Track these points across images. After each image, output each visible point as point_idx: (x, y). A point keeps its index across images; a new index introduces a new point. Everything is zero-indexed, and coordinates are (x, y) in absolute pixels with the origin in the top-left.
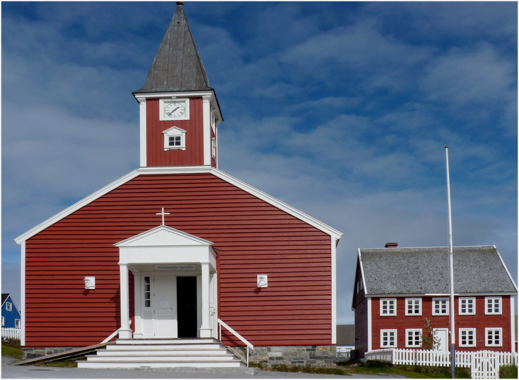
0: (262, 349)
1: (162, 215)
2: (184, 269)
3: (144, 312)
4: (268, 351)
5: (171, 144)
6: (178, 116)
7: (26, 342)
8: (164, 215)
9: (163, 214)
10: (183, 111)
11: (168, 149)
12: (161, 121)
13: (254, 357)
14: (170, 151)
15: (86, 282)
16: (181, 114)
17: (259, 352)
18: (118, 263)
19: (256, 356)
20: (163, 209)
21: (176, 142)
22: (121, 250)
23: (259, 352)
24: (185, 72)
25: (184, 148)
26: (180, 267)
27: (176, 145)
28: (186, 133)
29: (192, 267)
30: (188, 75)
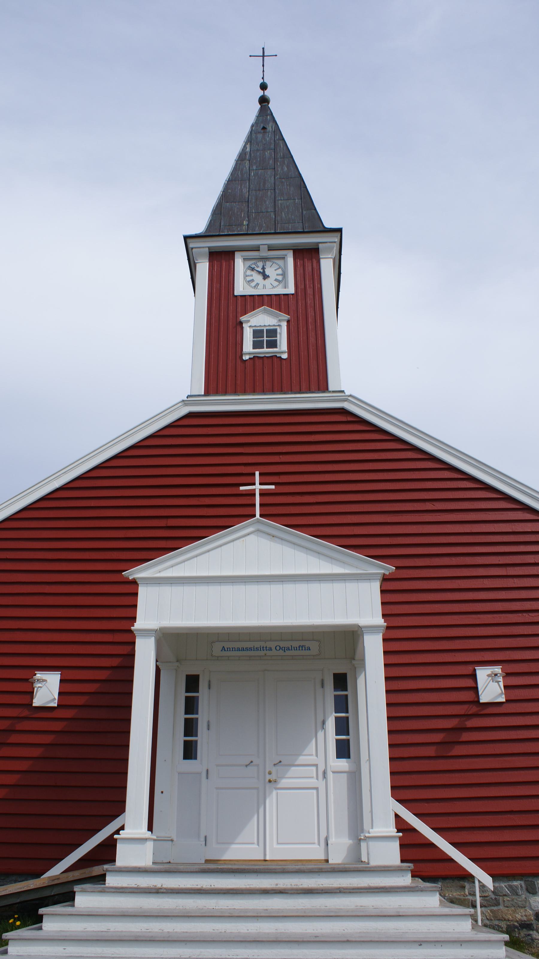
0: (511, 887)
1: (255, 490)
2: (288, 653)
3: (179, 773)
4: (530, 893)
5: (257, 345)
6: (271, 287)
7: (136, 594)
8: (260, 490)
9: (258, 487)
10: (280, 278)
11: (252, 356)
12: (236, 296)
13: (491, 911)
14: (255, 359)
15: (37, 685)
16: (277, 283)
17: (505, 895)
18: (132, 628)
19: (495, 908)
20: (257, 473)
21: (266, 340)
22: (142, 591)
23: (505, 895)
24: (281, 204)
25: (285, 352)
26: (278, 648)
27: (267, 348)
28: (288, 322)
29: (309, 649)
30: (286, 210)
